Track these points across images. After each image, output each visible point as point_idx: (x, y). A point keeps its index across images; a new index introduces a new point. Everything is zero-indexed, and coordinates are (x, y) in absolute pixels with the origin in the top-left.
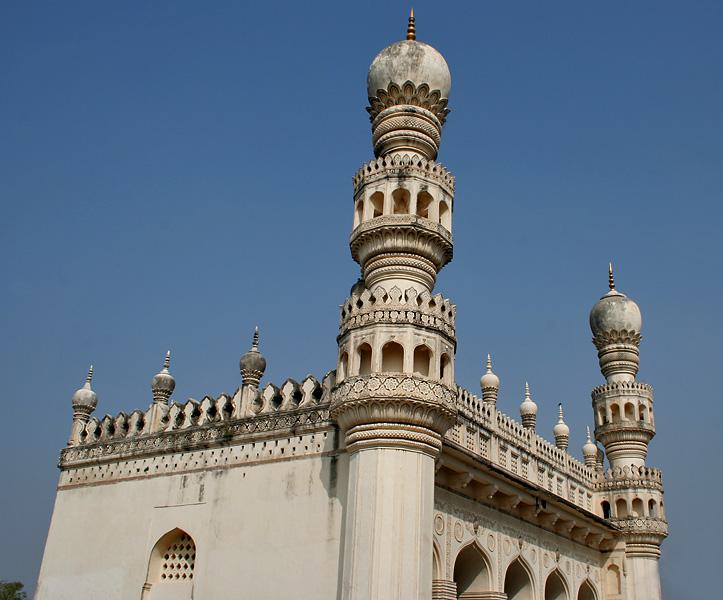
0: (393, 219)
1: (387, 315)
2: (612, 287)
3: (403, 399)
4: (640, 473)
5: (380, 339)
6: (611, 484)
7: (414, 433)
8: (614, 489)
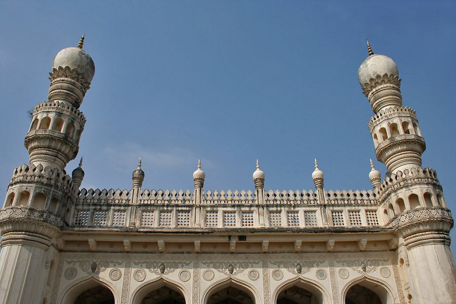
5: (404, 194)
7: (426, 236)
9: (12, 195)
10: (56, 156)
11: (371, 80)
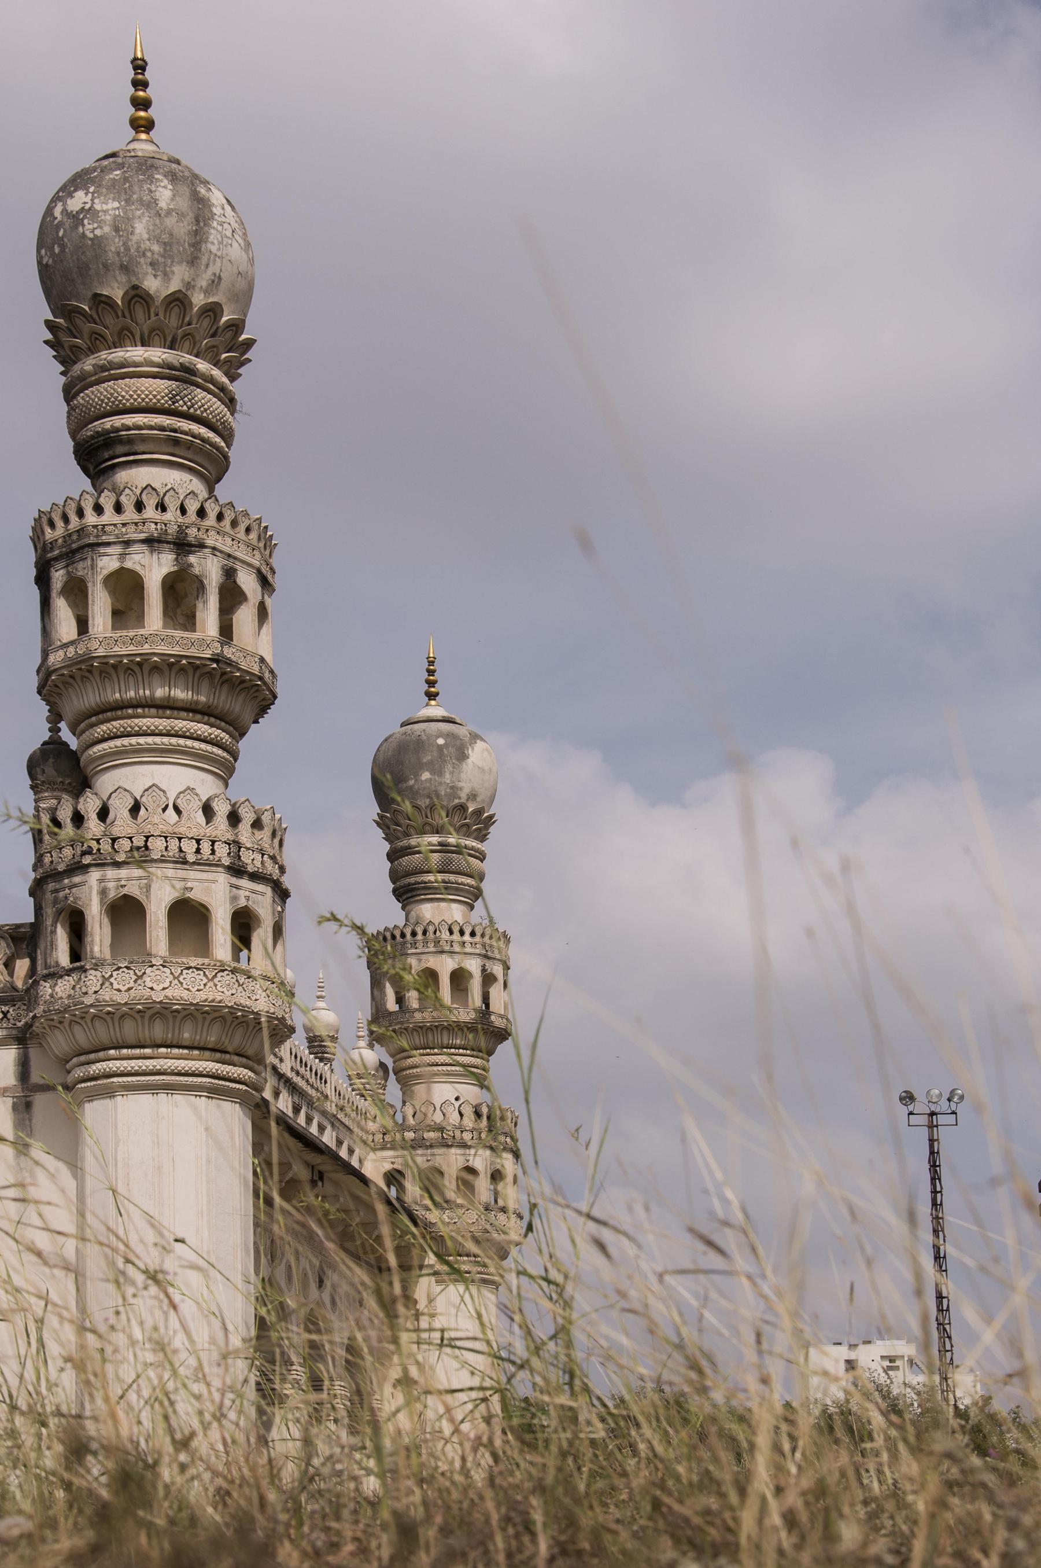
0: (171, 641)
1: (174, 844)
2: (431, 696)
3: (216, 1009)
6: (410, 1135)
8: (418, 1144)
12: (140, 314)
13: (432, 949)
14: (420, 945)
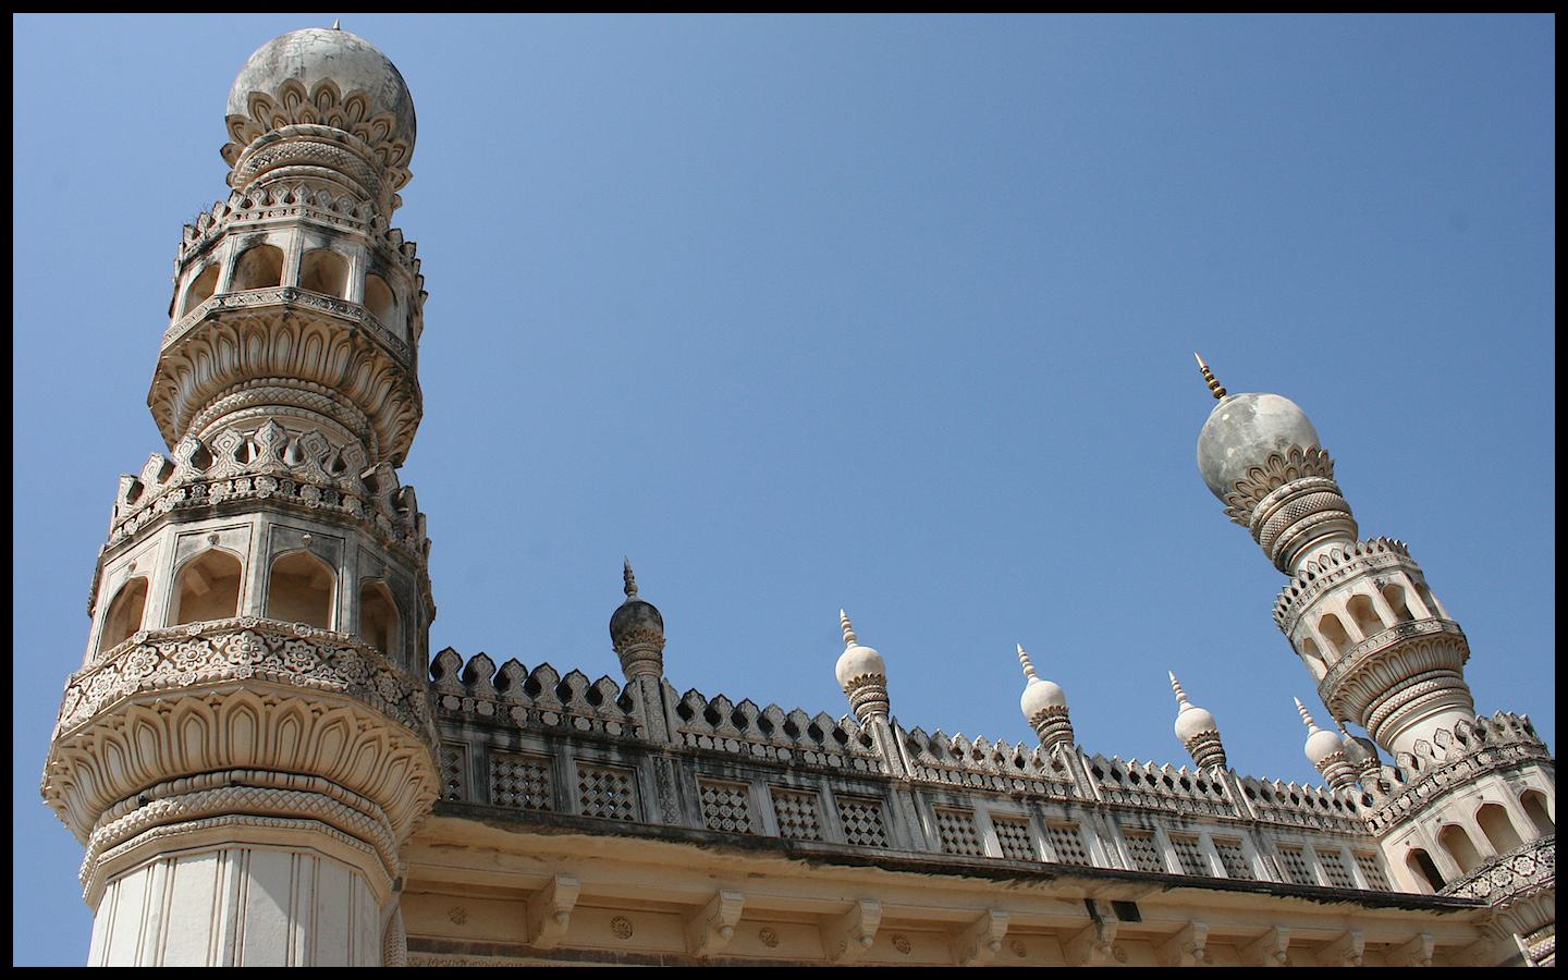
4: (1463, 740)
6: (1404, 802)
9: (135, 591)
10: (331, 415)
11: (1254, 470)
12: (1260, 478)
13: (1316, 596)
14: (1305, 599)
